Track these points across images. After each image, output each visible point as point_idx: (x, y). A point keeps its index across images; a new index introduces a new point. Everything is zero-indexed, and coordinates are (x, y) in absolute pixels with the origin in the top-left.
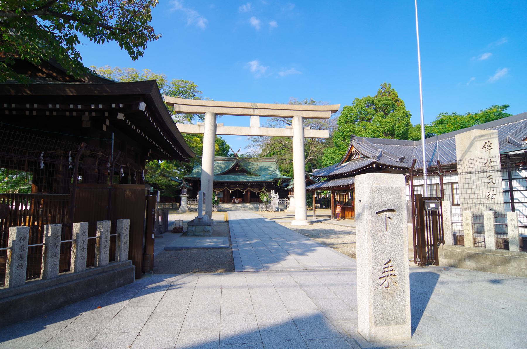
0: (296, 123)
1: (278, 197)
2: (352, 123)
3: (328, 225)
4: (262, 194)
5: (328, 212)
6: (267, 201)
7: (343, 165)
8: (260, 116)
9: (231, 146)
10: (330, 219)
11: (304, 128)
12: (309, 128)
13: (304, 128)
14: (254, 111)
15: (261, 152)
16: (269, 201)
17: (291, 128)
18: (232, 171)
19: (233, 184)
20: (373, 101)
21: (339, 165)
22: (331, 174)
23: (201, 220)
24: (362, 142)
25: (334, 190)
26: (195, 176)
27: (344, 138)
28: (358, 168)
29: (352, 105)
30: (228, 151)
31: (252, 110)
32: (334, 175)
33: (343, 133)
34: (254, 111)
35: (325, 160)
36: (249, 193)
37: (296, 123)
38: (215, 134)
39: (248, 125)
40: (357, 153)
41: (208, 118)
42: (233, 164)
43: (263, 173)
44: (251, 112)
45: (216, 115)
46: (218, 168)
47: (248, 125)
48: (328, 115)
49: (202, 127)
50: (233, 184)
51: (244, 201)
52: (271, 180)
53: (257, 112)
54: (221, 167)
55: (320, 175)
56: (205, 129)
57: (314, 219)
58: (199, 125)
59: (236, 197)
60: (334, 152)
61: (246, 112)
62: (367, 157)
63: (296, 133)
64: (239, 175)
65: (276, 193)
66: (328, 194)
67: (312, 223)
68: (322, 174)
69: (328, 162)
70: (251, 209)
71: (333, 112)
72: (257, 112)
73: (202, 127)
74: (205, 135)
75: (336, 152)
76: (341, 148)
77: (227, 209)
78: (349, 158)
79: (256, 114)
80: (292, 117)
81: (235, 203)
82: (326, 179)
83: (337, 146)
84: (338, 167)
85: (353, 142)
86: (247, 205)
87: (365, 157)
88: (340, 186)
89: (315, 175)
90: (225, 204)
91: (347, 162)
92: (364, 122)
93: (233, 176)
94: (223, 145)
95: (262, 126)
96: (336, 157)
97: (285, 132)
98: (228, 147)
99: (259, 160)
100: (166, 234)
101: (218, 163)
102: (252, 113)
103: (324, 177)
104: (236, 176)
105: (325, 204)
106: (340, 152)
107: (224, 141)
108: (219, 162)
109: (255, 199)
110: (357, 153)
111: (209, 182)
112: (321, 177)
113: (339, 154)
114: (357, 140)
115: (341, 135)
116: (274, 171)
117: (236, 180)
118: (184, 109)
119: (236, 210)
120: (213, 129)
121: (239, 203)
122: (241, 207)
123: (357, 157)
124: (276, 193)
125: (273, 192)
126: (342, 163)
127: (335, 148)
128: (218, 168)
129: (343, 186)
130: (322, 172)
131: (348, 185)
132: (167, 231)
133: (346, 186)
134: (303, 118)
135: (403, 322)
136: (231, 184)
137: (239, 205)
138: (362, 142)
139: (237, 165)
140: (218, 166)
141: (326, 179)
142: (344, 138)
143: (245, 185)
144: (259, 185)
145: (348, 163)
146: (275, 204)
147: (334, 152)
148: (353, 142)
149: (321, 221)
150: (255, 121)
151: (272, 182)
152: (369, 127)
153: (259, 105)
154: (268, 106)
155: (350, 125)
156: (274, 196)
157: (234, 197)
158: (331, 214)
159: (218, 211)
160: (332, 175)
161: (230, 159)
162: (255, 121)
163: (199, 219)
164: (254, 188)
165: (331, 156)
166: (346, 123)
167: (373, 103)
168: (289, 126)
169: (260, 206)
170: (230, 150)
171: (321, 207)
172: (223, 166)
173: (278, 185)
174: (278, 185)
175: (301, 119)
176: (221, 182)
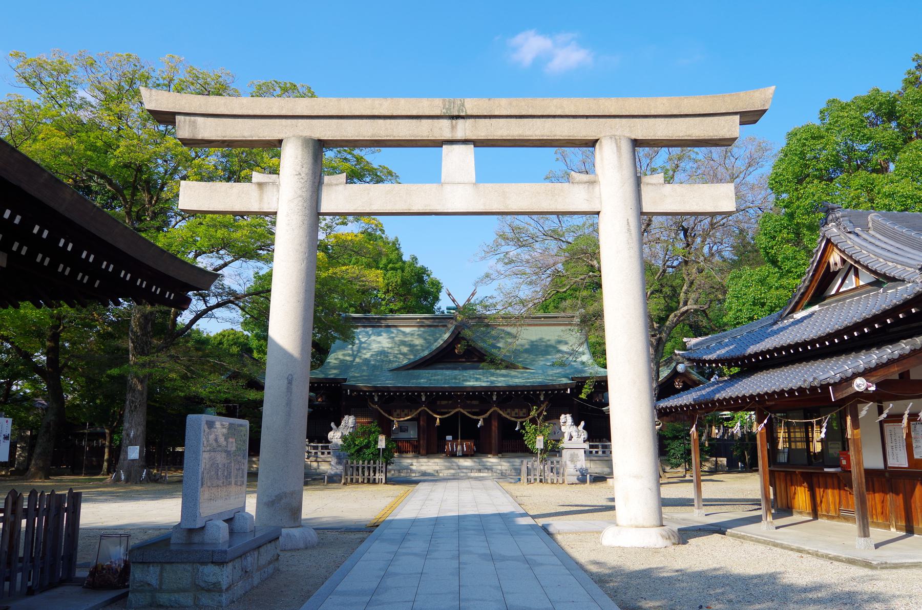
0: (611, 162)
1: (584, 435)
2: (821, 178)
3: (749, 546)
4: (530, 428)
5: (750, 485)
6: (544, 451)
7: (798, 315)
8: (477, 143)
9: (447, 284)
10: (758, 519)
11: (638, 182)
12: (659, 178)
13: (638, 182)
14: (453, 128)
15: (525, 292)
16: (553, 450)
17: (592, 183)
18: (443, 357)
19: (444, 397)
20: (892, 102)
21: (781, 318)
22: (752, 349)
23: (196, 539)
24: (866, 229)
25: (761, 404)
26: (333, 373)
27: (797, 234)
28: (857, 319)
29: (818, 123)
30: (437, 299)
31: (446, 123)
32: (763, 353)
33: (791, 216)
34: (453, 128)
35: (732, 307)
36: (495, 424)
37: (611, 162)
38: (315, 214)
39: (434, 176)
40: (852, 267)
41: (293, 159)
42: (446, 336)
43: (541, 362)
44: (443, 129)
45: (319, 146)
46: (405, 349)
47: (434, 176)
48: (729, 127)
49: (269, 190)
50: (444, 397)
51: (480, 450)
52: (565, 381)
53: (463, 129)
54: (411, 346)
55: (713, 356)
56: (280, 195)
57: (696, 516)
58: (260, 185)
59: (455, 438)
60: (762, 281)
61: (422, 130)
62: (893, 279)
63: (607, 197)
64: (465, 369)
65: (577, 424)
66: (743, 423)
67: (685, 535)
68: (722, 352)
69: (745, 315)
70: (503, 476)
71: (750, 117)
72: (463, 129)
73: (269, 191)
74: (280, 219)
75: (772, 280)
76: (787, 266)
77: (424, 474)
78: (820, 288)
79: (459, 135)
80: (592, 143)
81: (453, 455)
82: (735, 370)
83: (774, 262)
84: (780, 325)
85: (832, 230)
86: (492, 460)
87: (882, 280)
88: (791, 391)
89: (694, 356)
90: (423, 460)
91: (810, 304)
92: (863, 173)
93: (448, 372)
94: (420, 280)
95: (483, 176)
96: (772, 297)
97: (573, 197)
98: (437, 286)
99: (519, 320)
100: (67, 589)
101: (404, 334)
102: (447, 135)
103: (729, 361)
104: (456, 372)
105: (737, 456)
106: (784, 281)
107: (424, 270)
108: (408, 330)
109: (512, 443)
110: (852, 267)
111: (290, 382)
112: (716, 361)
113: (781, 286)
114: (845, 222)
115: (785, 222)
116: (573, 353)
117: (453, 383)
118: (208, 130)
119: (454, 478)
120: (307, 195)
121: (465, 455)
122: (471, 469)
123: (852, 282)
124: (577, 424)
125: (566, 420)
126: (793, 310)
127: (767, 268)
128: (405, 349)
129: (800, 390)
130: (721, 345)
131: (825, 387)
132: (69, 579)
133: (813, 389)
134: (636, 143)
135: (194, 122)
136: (439, 397)
137: (467, 462)
138: (866, 229)
139: (457, 338)
140: (403, 343)
141: (735, 370)
142: (797, 234)
143: (481, 398)
144: (522, 398)
145: (816, 308)
146: (573, 459)
147: (762, 281)
148: (832, 230)
149: (719, 529)
150: (459, 161)
151: (566, 386)
152: (886, 189)
153: (471, 106)
154: (502, 106)
155: (814, 188)
156: (572, 433)
157: (449, 438)
158: (758, 495)
159: (388, 481)
160: (756, 355)
161: (443, 320)
162: (459, 161)
163: (191, 531)
164: (513, 409)
165: (752, 292)
166: (800, 182)
167: (888, 111)
168: (584, 177)
169: (526, 463)
170: (443, 295)
171: (732, 468)
172: (418, 342)
173: (583, 396)
174: (583, 396)
175: (626, 147)
176: (407, 390)
